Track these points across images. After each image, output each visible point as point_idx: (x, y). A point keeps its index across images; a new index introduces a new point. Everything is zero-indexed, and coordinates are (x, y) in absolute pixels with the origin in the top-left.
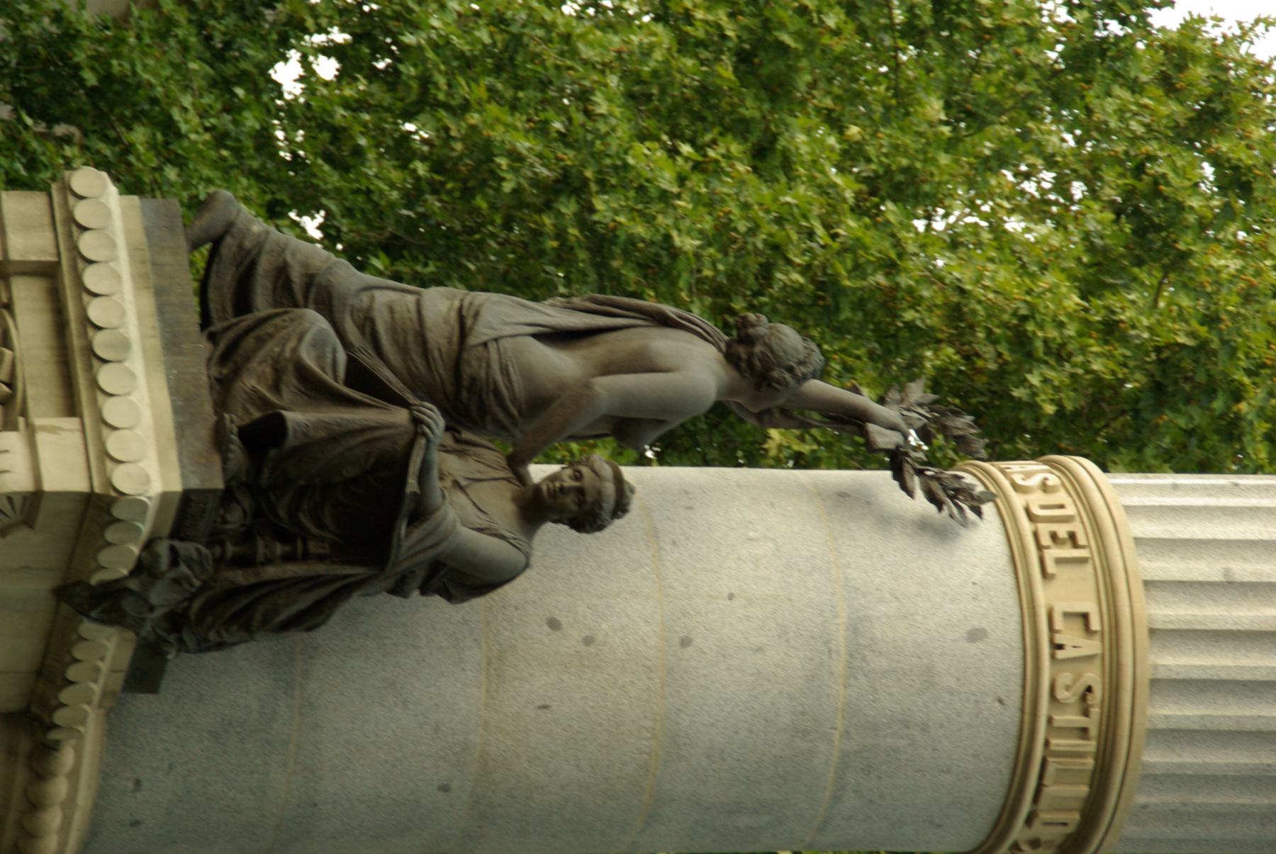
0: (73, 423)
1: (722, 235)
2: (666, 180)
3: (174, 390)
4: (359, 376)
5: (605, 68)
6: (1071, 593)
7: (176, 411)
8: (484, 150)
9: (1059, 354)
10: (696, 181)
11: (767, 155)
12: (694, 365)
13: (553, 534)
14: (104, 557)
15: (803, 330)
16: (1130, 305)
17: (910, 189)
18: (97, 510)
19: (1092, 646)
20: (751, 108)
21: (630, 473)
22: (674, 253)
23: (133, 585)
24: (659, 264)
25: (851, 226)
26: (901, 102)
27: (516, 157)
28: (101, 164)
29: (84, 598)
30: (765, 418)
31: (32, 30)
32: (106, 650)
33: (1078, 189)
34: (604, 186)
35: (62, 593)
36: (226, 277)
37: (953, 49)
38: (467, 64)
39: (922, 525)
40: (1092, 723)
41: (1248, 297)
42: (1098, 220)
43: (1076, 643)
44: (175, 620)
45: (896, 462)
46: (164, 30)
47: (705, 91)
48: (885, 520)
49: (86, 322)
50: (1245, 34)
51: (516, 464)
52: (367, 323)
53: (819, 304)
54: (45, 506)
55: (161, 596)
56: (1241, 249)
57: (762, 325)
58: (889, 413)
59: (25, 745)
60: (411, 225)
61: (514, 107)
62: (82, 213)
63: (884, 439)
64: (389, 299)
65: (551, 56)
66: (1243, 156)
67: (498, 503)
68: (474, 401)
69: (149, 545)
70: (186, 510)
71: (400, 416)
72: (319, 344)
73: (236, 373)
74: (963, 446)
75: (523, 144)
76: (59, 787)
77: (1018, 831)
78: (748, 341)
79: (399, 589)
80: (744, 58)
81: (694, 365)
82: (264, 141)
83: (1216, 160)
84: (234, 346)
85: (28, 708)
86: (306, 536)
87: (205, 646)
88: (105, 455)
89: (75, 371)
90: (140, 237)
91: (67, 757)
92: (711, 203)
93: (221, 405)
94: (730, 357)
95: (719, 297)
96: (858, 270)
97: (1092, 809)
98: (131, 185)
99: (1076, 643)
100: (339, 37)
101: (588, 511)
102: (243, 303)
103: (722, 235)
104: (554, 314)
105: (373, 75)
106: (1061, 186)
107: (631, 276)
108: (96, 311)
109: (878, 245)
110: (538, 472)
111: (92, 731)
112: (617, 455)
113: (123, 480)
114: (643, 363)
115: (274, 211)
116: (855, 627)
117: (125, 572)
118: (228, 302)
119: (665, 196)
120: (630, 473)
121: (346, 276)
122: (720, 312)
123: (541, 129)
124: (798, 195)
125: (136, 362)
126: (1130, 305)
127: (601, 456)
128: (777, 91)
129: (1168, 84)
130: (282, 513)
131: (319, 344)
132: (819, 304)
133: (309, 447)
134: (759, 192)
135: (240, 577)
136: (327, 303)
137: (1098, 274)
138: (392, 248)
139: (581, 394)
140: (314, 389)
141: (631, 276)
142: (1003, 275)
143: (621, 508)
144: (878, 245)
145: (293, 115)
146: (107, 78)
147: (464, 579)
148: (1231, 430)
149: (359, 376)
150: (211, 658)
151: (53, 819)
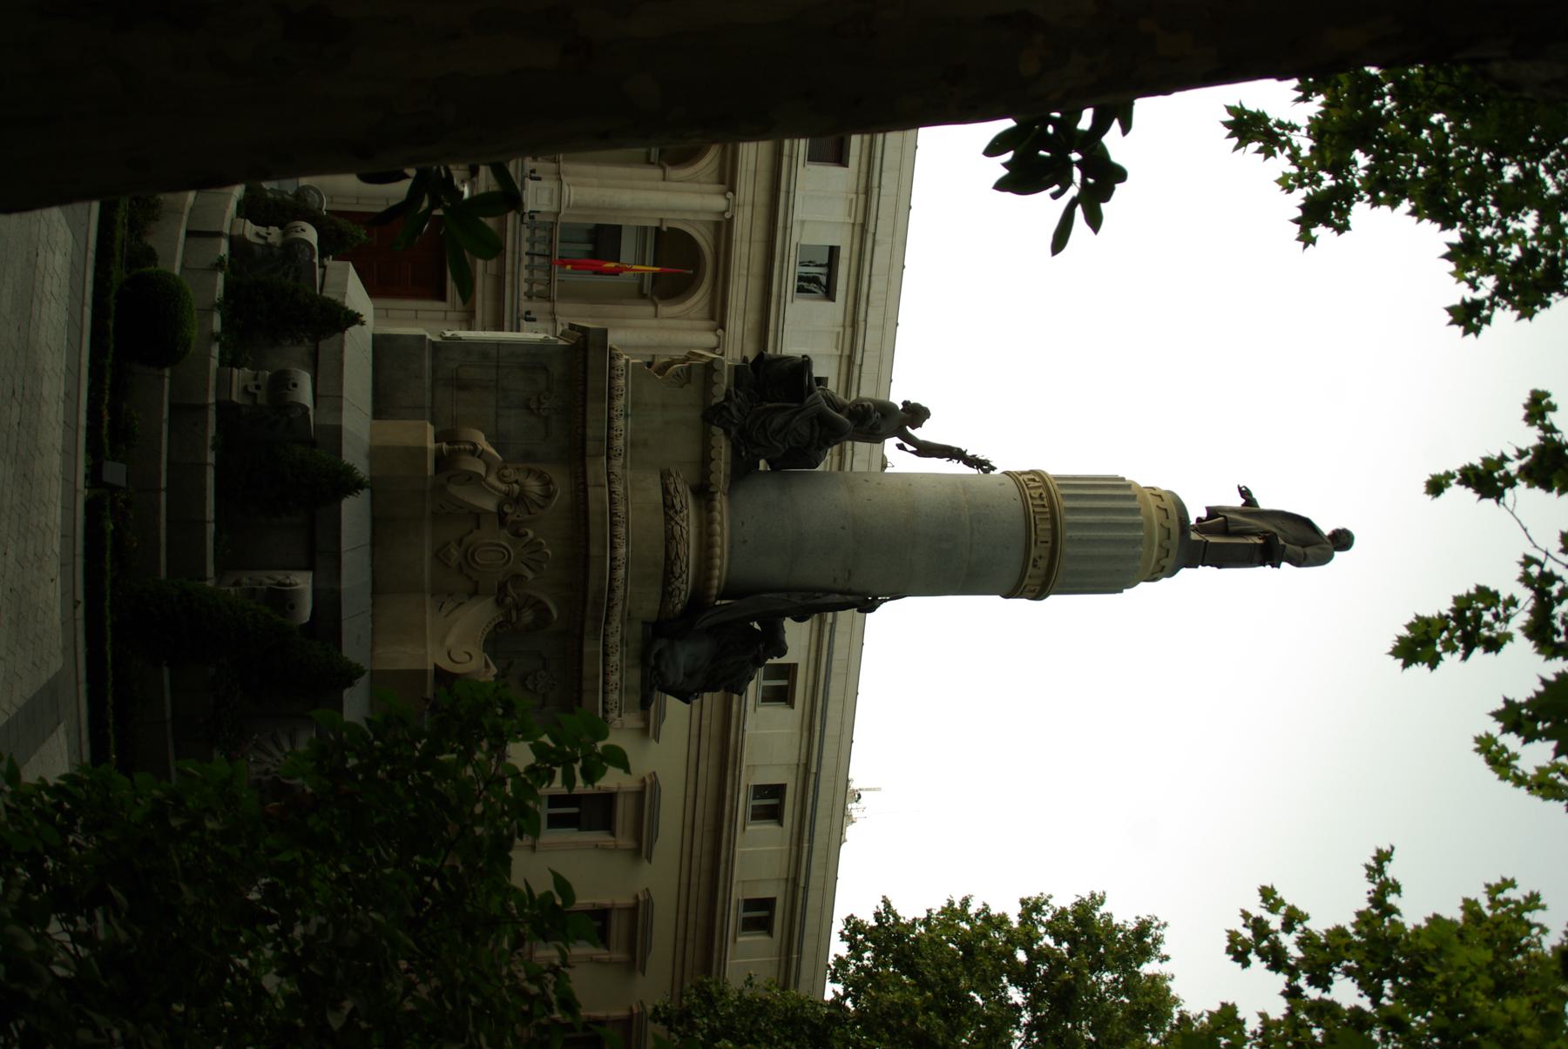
29: (712, 415)
40: (1045, 502)
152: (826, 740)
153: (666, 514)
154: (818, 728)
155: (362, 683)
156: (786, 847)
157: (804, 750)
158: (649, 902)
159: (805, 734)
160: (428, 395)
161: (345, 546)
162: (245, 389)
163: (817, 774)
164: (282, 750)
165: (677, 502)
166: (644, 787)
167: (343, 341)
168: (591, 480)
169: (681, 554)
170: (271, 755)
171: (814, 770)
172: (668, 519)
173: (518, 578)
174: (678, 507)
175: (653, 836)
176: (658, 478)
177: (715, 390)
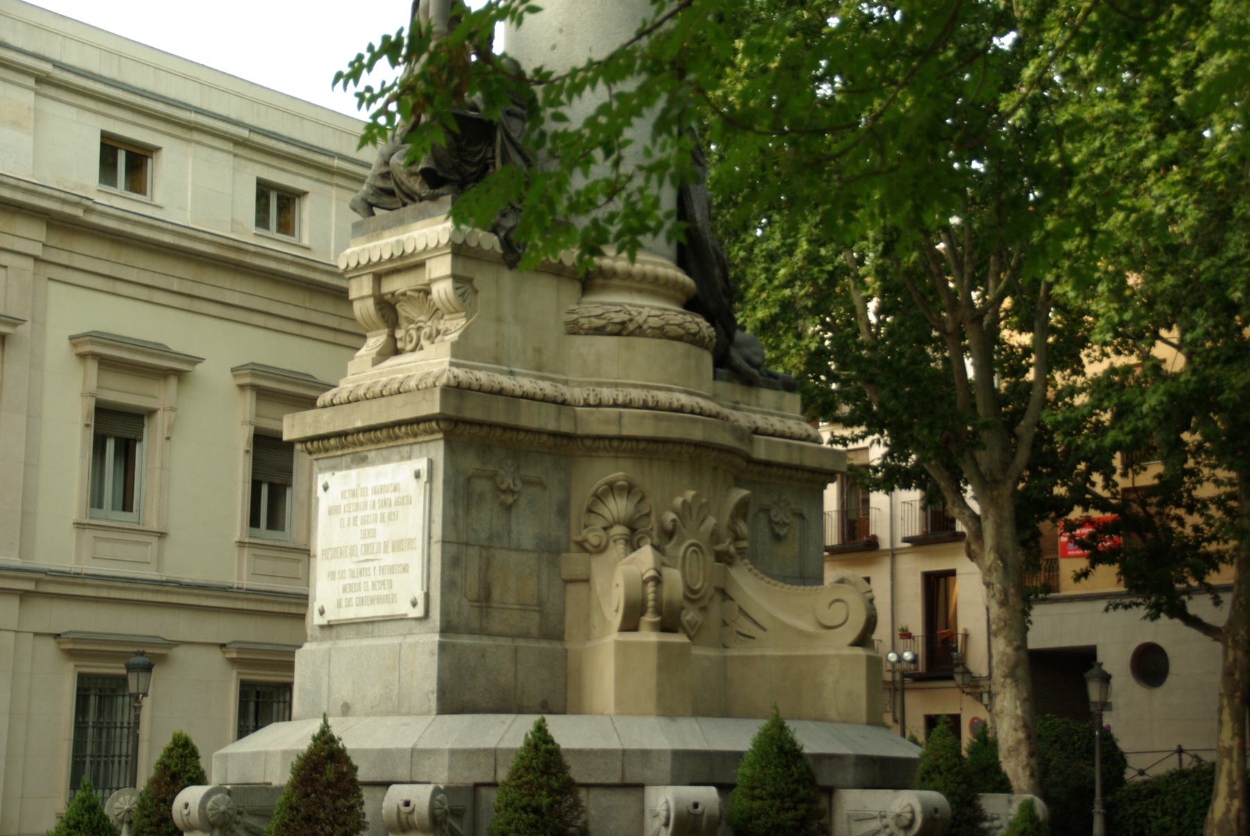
0: (428, 263)
3: (417, 219)
7: (424, 218)
14: (486, 246)
18: (459, 250)
23: (502, 234)
29: (511, 255)
35: (512, 265)
36: (386, 200)
49: (391, 259)
54: (460, 272)
59: (600, 281)
62: (353, 264)
70: (458, 216)
84: (408, 196)
85: (580, 280)
86: (484, 158)
88: (436, 248)
89: (410, 264)
90: (363, 239)
102: (390, 193)
108: (386, 256)
113: (444, 240)
117: (496, 238)
130: (474, 169)
152: (205, 106)
153: (631, 334)
154: (192, 117)
156: (334, 191)
157: (217, 143)
158: (256, 369)
159: (196, 136)
160: (501, 641)
161: (614, 744)
163: (252, 129)
165: (619, 318)
166: (94, 356)
167: (568, 750)
168: (612, 430)
169: (599, 311)
171: (245, 133)
172: (639, 332)
173: (715, 537)
174: (626, 317)
175: (161, 350)
176: (579, 340)
177: (486, 246)
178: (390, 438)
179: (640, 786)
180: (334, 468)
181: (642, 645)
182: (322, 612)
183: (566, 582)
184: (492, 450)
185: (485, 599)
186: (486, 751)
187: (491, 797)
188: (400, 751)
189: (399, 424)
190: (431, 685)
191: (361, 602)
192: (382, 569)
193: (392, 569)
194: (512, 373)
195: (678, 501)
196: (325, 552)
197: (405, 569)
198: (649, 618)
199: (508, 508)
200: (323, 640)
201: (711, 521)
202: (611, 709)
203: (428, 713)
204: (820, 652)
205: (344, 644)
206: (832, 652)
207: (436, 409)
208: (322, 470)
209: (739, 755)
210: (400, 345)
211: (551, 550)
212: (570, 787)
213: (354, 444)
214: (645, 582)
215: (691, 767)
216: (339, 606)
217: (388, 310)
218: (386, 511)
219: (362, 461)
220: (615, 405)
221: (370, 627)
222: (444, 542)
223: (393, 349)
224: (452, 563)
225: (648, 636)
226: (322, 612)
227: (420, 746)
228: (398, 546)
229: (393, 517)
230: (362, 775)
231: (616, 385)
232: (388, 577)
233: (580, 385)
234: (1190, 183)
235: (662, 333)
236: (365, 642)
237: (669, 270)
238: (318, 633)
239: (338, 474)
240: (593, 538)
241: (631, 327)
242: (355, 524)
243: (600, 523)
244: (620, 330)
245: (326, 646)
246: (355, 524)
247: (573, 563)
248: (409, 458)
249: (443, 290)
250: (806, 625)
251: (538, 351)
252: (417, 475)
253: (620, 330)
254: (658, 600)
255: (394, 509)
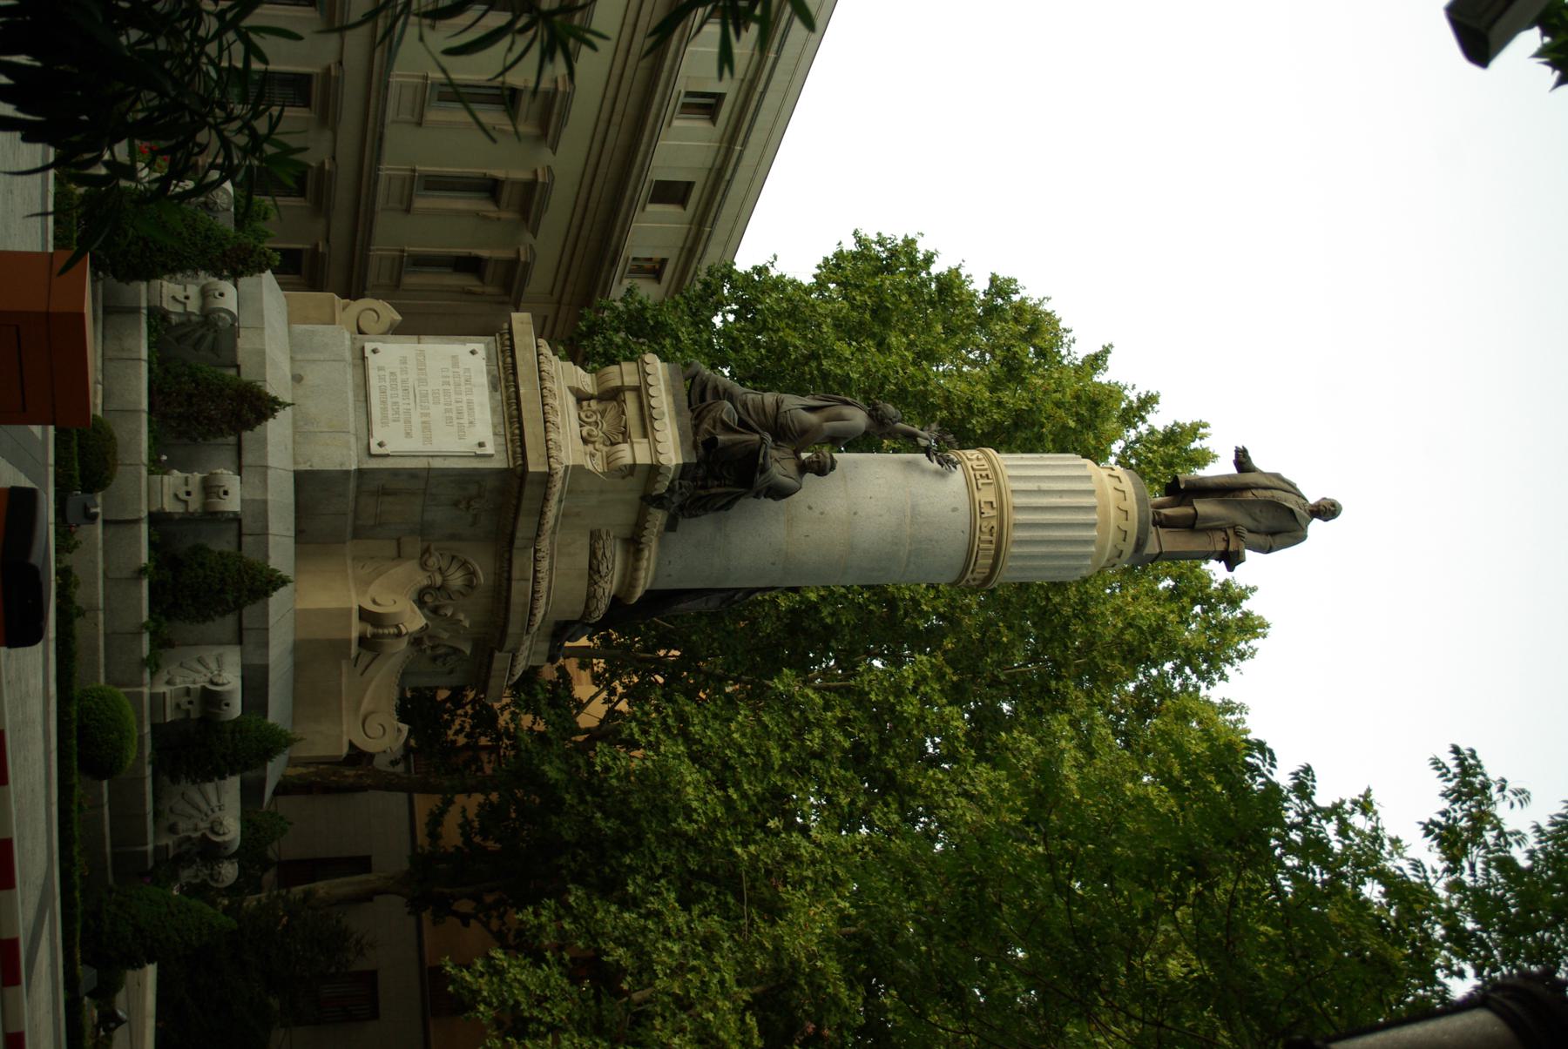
1: (867, 373)
2: (847, 354)
4: (742, 423)
5: (826, 316)
6: (987, 495)
8: (785, 345)
9: (982, 413)
10: (858, 355)
11: (882, 346)
12: (858, 418)
13: (809, 477)
15: (895, 406)
16: (1006, 396)
17: (931, 356)
18: (654, 470)
19: (994, 513)
20: (876, 329)
21: (836, 456)
22: (851, 379)
24: (845, 383)
25: (911, 369)
26: (928, 326)
27: (796, 347)
28: (655, 352)
29: (650, 500)
30: (882, 436)
31: (632, 307)
32: (658, 518)
33: (988, 356)
34: (826, 357)
35: (643, 498)
36: (697, 389)
37: (945, 309)
38: (778, 315)
39: (936, 472)
40: (994, 539)
41: (1045, 392)
42: (995, 367)
43: (988, 512)
44: (681, 507)
45: (927, 451)
46: (676, 306)
47: (861, 323)
48: (924, 471)
50: (1041, 302)
51: (797, 453)
52: (745, 405)
53: (900, 396)
55: (676, 499)
56: (1043, 377)
57: (880, 404)
58: (925, 434)
60: (760, 371)
61: (795, 329)
62: (648, 369)
63: (923, 443)
64: (753, 397)
65: (808, 312)
66: (1043, 345)
67: (791, 466)
68: (783, 432)
69: (672, 482)
70: (684, 469)
71: (757, 437)
72: (728, 413)
73: (701, 422)
74: (950, 445)
75: (798, 343)
76: (644, 564)
77: (969, 576)
78: (876, 410)
79: (757, 496)
80: (874, 312)
81: (858, 418)
82: (710, 342)
83: (1034, 346)
87: (691, 516)
91: (646, 553)
92: (863, 362)
93: (696, 434)
94: (870, 415)
95: (866, 395)
96: (914, 384)
97: (993, 568)
98: (664, 359)
99: (988, 512)
100: (735, 307)
101: (822, 469)
102: (702, 398)
103: (867, 373)
104: (809, 401)
105: (746, 319)
106: (982, 355)
107: (836, 387)
108: (653, 402)
109: (920, 376)
110: (804, 456)
111: (654, 545)
112: (831, 450)
113: (663, 459)
114: (840, 418)
115: (713, 367)
116: (913, 508)
118: (698, 399)
119: (847, 360)
120: (836, 456)
121: (738, 389)
122: (866, 399)
123: (804, 337)
124: (893, 359)
125: (667, 419)
126: (1006, 396)
127: (826, 450)
128: (885, 323)
129: (1016, 321)
131: (728, 413)
132: (900, 396)
133: (727, 447)
134: (879, 358)
135: (703, 492)
136: (731, 397)
137: (995, 385)
138: (754, 379)
139: (818, 429)
140: (727, 428)
141: (836, 387)
142: (964, 386)
143: (833, 468)
144: (920, 376)
145: (720, 333)
146: (657, 322)
147: (780, 493)
148: (1040, 438)
149: (742, 423)
150: (693, 520)
151: (642, 574)
153: (590, 576)
155: (283, 416)
160: (352, 505)
162: (178, 706)
164: (208, 803)
165: (603, 569)
167: (267, 605)
168: (516, 574)
169: (608, 554)
170: (198, 672)
172: (592, 582)
176: (586, 541)
178: (511, 417)
179: (240, 642)
180: (488, 358)
181: (349, 626)
182: (374, 351)
183: (398, 540)
184: (500, 501)
185: (384, 492)
186: (266, 527)
187: (232, 372)
188: (265, 457)
189: (521, 428)
190: (318, 465)
191: (383, 391)
192: (408, 411)
193: (408, 421)
194: (560, 501)
195: (461, 616)
196: (422, 353)
197: (408, 435)
198: (369, 630)
199: (456, 504)
200: (353, 349)
201: (445, 635)
202: (301, 605)
203: (295, 462)
204: (345, 719)
205: (349, 370)
206: (345, 728)
207: (531, 469)
208: (487, 345)
209: (265, 715)
210: (585, 403)
211: (423, 530)
212: (238, 607)
213: (507, 380)
214: (397, 626)
215: (255, 683)
216: (380, 369)
217: (613, 395)
218: (454, 415)
219: (494, 387)
220: (535, 571)
221: (362, 398)
222: (429, 470)
223: (581, 397)
224: (413, 474)
225: (356, 629)
226: (374, 351)
227: (270, 472)
228: (426, 426)
229: (449, 421)
230: (246, 435)
231: (551, 569)
232: (402, 417)
233: (552, 543)
234: (715, 822)
235: (591, 597)
236: (350, 395)
237: (643, 583)
238: (358, 345)
239: (484, 363)
240: (433, 561)
241: (596, 577)
242: (444, 383)
243: (444, 564)
244: (594, 570)
245: (348, 355)
246: (444, 383)
247: (413, 546)
248: (495, 434)
249: (625, 454)
250: (366, 705)
251: (578, 514)
252: (481, 445)
253: (594, 570)
254: (383, 636)
255: (455, 422)
